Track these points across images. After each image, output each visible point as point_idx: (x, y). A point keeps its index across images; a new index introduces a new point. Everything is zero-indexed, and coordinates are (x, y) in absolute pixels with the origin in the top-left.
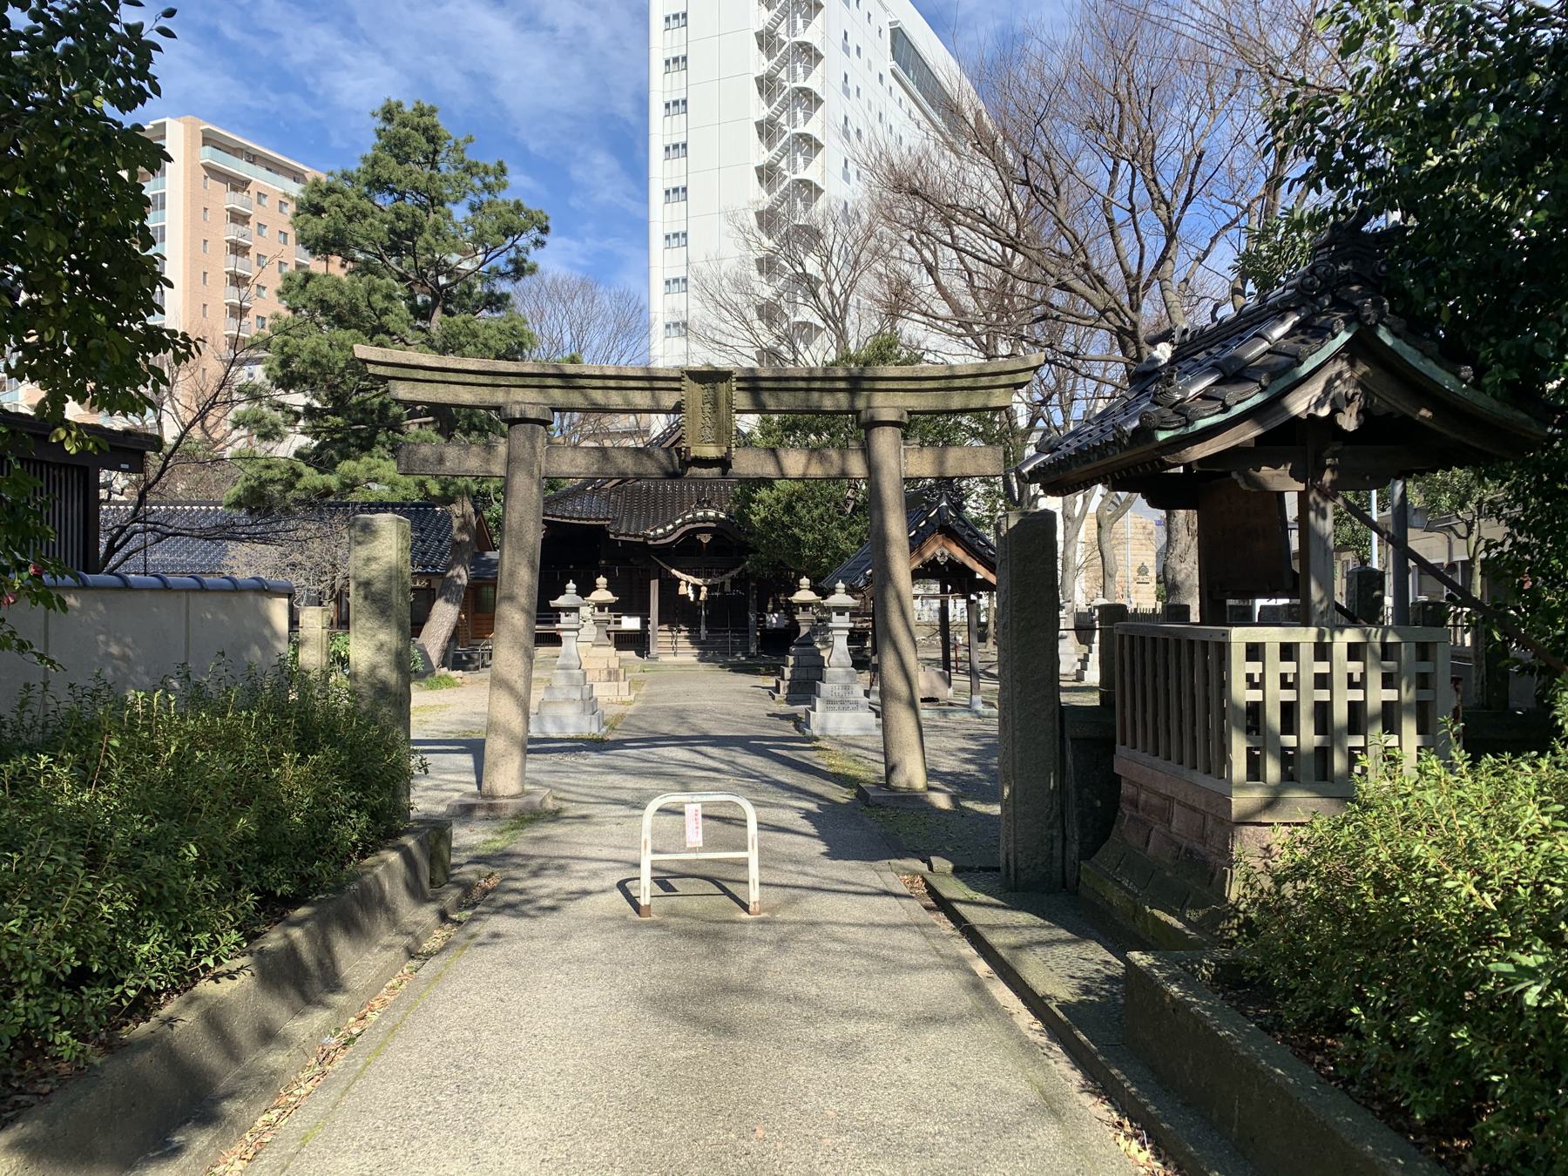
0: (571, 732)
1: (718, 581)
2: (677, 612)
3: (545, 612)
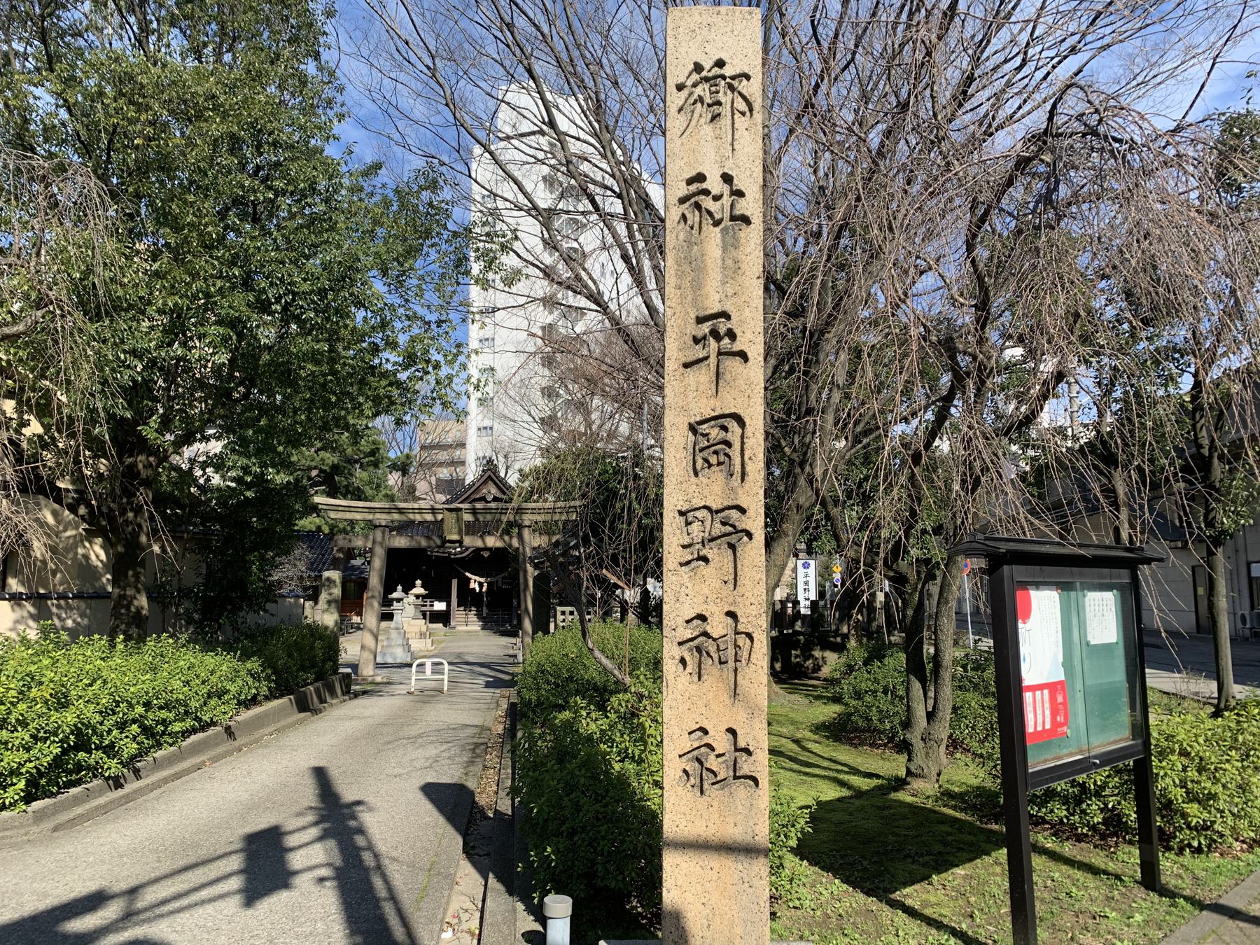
0: (399, 661)
1: (494, 580)
2: (468, 599)
3: (387, 602)
